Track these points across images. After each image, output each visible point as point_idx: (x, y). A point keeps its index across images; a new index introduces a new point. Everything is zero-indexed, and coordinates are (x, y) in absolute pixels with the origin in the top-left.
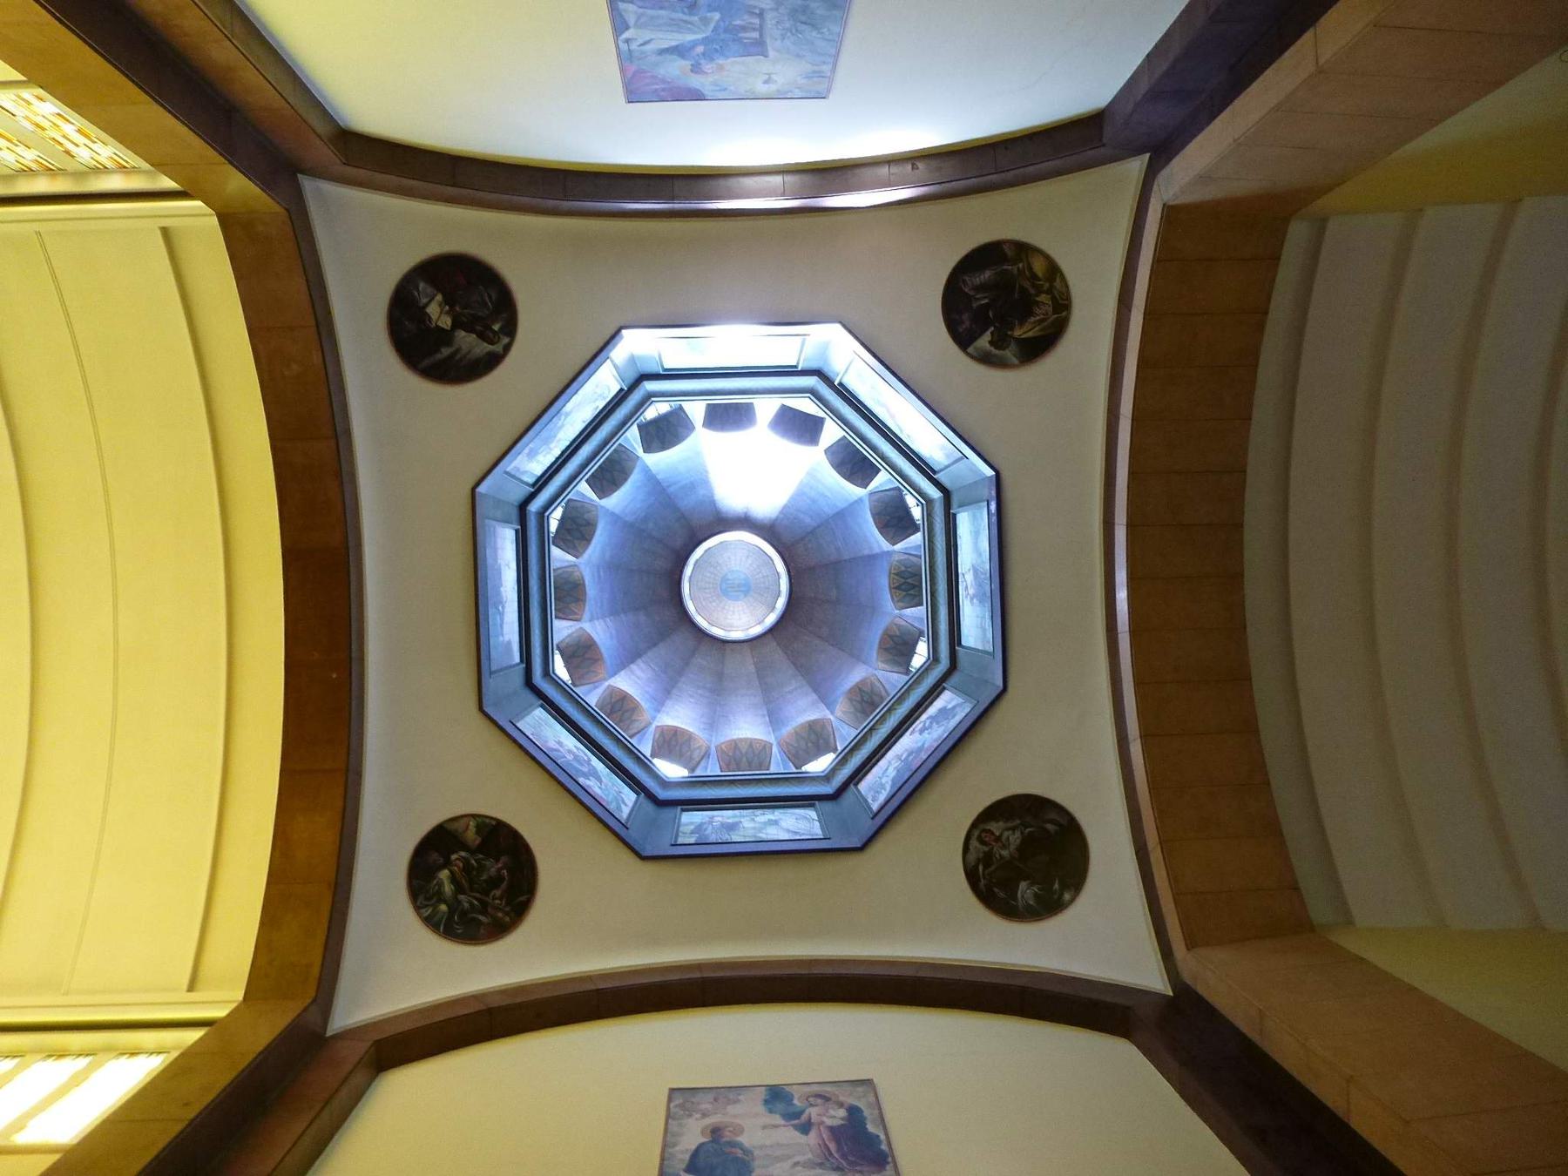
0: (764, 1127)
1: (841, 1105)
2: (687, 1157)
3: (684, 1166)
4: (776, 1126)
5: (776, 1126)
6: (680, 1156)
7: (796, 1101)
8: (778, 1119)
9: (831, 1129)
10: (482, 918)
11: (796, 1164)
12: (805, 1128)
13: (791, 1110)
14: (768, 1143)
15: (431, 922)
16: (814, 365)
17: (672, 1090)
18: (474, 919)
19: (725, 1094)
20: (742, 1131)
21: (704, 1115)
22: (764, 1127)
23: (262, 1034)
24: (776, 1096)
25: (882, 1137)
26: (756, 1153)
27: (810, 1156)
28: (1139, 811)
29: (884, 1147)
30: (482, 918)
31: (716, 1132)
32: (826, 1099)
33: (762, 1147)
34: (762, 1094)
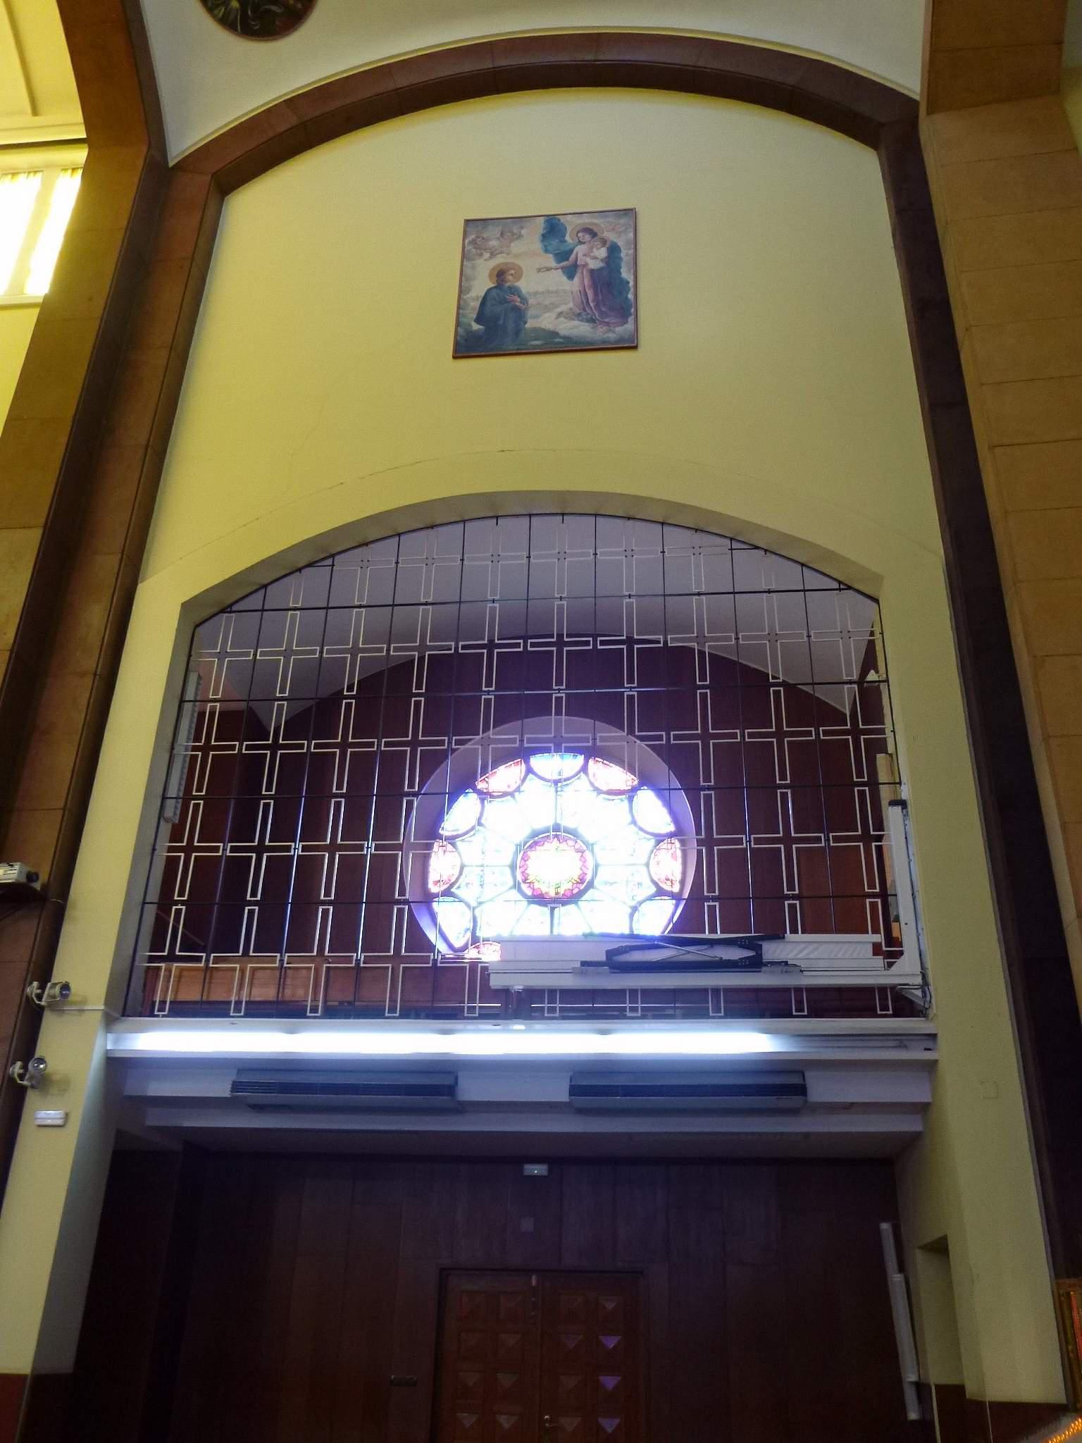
0: (539, 270)
1: (604, 242)
2: (477, 304)
3: (474, 316)
4: (549, 269)
5: (549, 269)
6: (472, 304)
7: (567, 238)
8: (550, 261)
9: (592, 271)
10: (274, 8)
11: (560, 314)
12: (570, 272)
13: (564, 248)
14: (541, 289)
15: (228, 22)
16: (193, 626)
17: (467, 222)
18: (269, 11)
19: (511, 226)
20: (519, 274)
21: (493, 255)
22: (539, 270)
23: (129, 182)
24: (553, 228)
25: (631, 284)
26: (531, 301)
27: (571, 305)
28: (758, 1086)
29: (630, 296)
30: (274, 8)
31: (500, 274)
32: (593, 234)
33: (536, 293)
34: (540, 225)
